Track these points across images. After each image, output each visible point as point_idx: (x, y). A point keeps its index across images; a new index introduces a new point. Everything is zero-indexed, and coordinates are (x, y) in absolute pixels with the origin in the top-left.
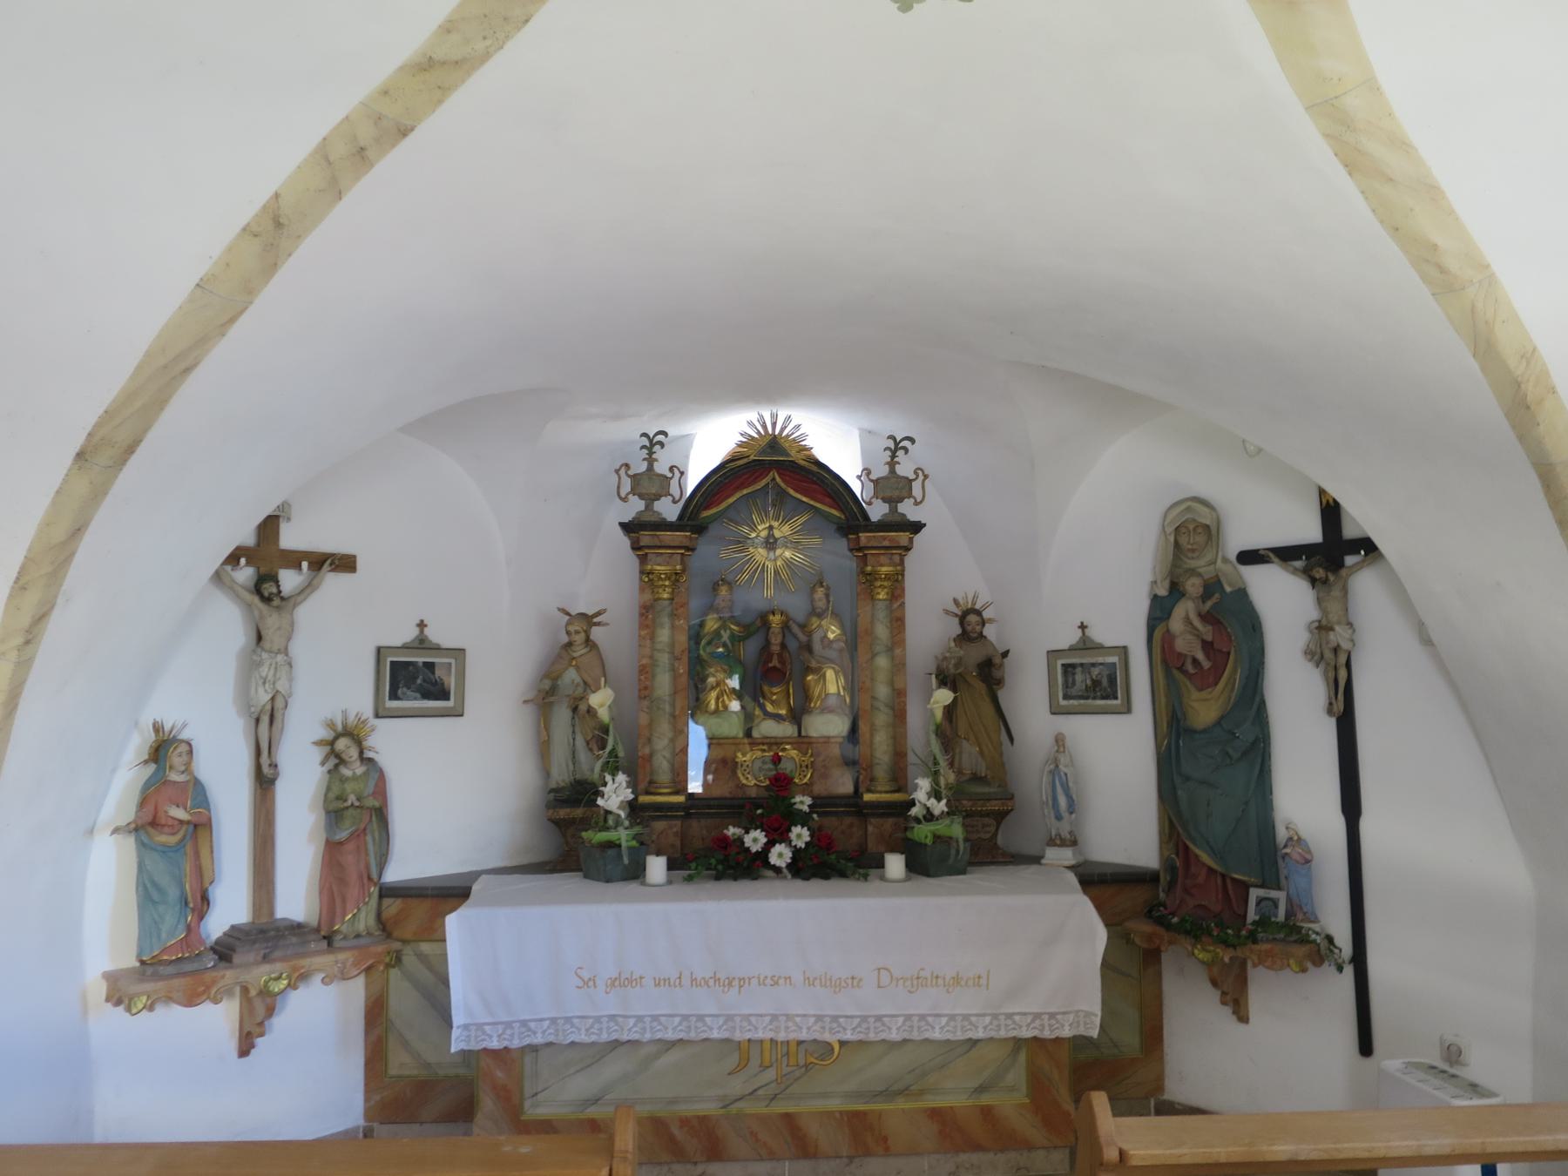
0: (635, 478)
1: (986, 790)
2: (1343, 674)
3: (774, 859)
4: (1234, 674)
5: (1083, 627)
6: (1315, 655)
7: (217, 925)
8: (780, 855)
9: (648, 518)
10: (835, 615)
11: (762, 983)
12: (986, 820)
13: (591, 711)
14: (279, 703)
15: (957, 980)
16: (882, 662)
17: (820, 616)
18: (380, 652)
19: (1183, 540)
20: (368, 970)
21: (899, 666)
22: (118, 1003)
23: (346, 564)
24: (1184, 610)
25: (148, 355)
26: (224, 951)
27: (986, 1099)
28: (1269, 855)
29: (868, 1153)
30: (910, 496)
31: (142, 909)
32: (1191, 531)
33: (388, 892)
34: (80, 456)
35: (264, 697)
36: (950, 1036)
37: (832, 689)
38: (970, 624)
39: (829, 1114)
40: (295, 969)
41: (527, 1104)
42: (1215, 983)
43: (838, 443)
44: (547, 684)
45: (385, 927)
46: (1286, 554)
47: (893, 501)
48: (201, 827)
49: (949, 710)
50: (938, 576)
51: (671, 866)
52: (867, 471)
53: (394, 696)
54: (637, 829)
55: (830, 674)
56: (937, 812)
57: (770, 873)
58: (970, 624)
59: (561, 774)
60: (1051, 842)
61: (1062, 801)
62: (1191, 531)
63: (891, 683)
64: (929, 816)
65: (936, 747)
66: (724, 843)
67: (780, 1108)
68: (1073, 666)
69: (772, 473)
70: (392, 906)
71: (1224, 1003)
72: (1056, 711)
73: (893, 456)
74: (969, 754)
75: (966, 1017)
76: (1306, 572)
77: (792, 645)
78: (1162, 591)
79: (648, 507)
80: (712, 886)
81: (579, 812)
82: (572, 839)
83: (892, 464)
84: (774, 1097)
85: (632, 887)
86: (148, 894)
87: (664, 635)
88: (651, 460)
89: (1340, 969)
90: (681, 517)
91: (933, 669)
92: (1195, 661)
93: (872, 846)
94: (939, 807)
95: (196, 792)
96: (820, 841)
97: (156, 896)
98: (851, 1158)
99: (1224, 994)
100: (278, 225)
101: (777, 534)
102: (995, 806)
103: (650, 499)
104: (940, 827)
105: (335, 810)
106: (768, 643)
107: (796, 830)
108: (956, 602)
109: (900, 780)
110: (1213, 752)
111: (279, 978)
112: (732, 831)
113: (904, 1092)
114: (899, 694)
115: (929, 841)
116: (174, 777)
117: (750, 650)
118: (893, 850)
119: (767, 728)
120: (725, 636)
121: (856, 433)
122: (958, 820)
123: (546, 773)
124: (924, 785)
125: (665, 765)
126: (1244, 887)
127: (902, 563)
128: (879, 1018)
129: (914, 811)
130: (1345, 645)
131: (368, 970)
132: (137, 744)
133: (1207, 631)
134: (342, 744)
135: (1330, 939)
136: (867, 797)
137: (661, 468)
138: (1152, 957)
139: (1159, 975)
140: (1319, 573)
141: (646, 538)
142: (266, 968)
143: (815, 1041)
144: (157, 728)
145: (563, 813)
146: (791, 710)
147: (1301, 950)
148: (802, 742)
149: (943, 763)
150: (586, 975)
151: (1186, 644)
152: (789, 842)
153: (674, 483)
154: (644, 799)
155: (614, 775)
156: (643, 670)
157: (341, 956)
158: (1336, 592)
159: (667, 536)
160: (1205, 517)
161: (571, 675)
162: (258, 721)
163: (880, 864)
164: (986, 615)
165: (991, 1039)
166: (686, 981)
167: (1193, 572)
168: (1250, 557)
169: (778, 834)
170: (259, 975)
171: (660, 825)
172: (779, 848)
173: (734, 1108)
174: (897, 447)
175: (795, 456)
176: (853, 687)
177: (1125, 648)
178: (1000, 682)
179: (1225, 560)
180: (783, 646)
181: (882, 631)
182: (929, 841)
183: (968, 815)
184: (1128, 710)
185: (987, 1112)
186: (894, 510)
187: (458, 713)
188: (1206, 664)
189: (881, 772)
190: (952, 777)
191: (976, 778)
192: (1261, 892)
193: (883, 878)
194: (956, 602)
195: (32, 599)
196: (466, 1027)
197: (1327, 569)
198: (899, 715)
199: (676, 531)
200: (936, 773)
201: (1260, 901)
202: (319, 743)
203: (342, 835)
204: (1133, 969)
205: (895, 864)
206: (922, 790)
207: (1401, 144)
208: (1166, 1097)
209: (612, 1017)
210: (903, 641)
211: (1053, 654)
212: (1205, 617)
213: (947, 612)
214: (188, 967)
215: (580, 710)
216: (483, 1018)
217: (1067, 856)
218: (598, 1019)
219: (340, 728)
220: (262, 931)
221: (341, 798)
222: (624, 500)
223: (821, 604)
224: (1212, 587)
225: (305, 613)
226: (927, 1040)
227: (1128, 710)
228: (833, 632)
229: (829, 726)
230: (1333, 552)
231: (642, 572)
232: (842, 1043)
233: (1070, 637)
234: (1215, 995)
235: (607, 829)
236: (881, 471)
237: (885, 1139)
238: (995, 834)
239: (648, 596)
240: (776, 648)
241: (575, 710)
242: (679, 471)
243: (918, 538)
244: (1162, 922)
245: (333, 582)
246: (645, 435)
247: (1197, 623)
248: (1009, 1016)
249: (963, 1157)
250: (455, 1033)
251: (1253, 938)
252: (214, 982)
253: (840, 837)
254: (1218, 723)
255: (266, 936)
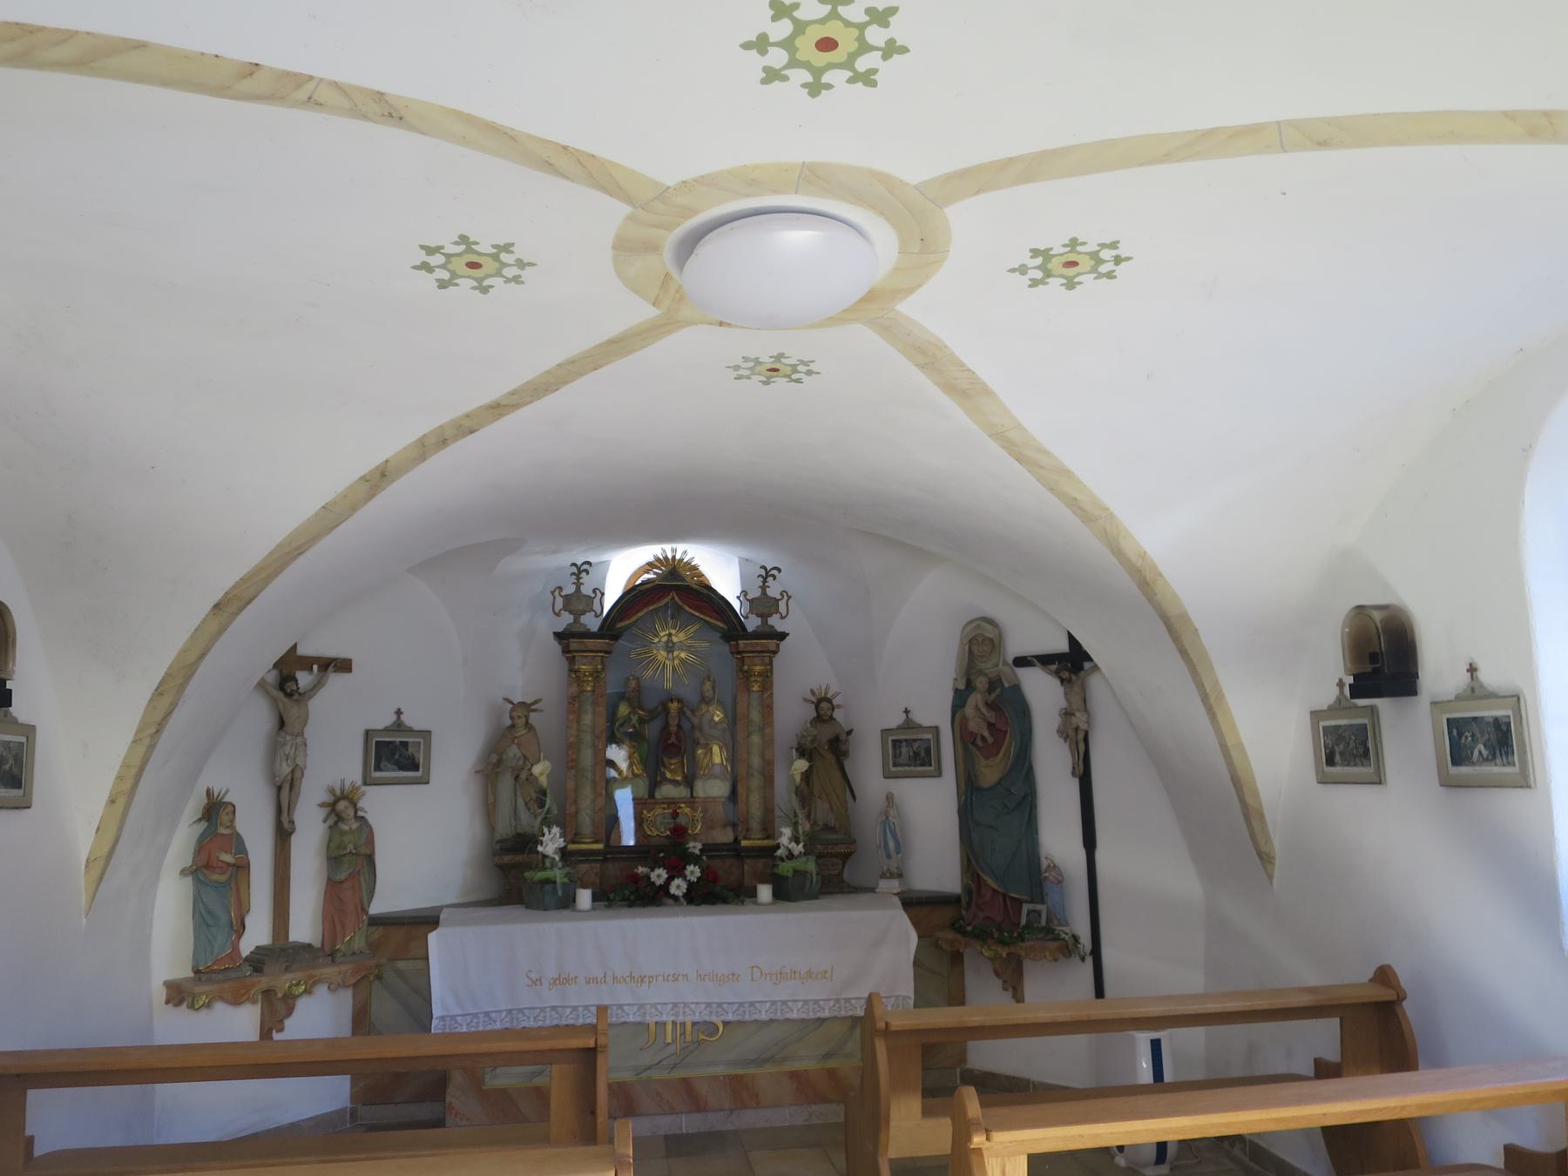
0: (567, 598)
1: (834, 836)
2: (1082, 746)
3: (673, 890)
4: (1010, 746)
5: (906, 711)
6: (1063, 733)
7: (247, 946)
8: (678, 887)
9: (576, 629)
10: (720, 703)
11: (666, 979)
12: (835, 860)
13: (531, 779)
14: (298, 774)
15: (809, 974)
16: (756, 739)
17: (708, 703)
18: (368, 734)
19: (974, 649)
20: (355, 985)
21: (768, 742)
22: (178, 1004)
23: (344, 666)
24: (975, 699)
25: (280, 545)
26: (258, 961)
27: (831, 1064)
28: (1035, 877)
29: (745, 1107)
30: (777, 611)
31: (196, 929)
32: (981, 642)
33: (376, 921)
34: (217, 606)
35: (286, 769)
36: (804, 1016)
37: (717, 760)
38: (823, 707)
39: (715, 1078)
40: (310, 977)
41: (487, 1078)
42: (997, 974)
43: (723, 572)
44: (494, 758)
45: (374, 947)
46: (1045, 660)
47: (764, 617)
48: (242, 868)
49: (807, 776)
50: (801, 670)
51: (595, 898)
52: (744, 593)
53: (378, 768)
54: (568, 869)
55: (716, 749)
56: (796, 853)
57: (670, 901)
58: (823, 707)
59: (504, 829)
60: (883, 876)
61: (891, 844)
62: (981, 642)
63: (762, 755)
64: (791, 856)
65: (796, 804)
66: (636, 879)
67: (679, 1074)
68: (900, 741)
69: (673, 591)
70: (378, 932)
71: (1005, 989)
72: (888, 775)
73: (765, 581)
74: (822, 810)
75: (816, 1002)
76: (1057, 673)
77: (686, 726)
78: (962, 687)
79: (576, 620)
80: (625, 911)
81: (519, 858)
82: (514, 877)
83: (764, 588)
84: (675, 1066)
85: (565, 913)
86: (203, 918)
87: (587, 719)
88: (578, 585)
89: (1083, 959)
90: (601, 628)
91: (795, 745)
92: (983, 738)
93: (747, 881)
94: (798, 849)
95: (237, 843)
96: (708, 876)
97: (210, 921)
98: (732, 1111)
99: (1005, 982)
100: (383, 475)
101: (675, 639)
102: (841, 849)
103: (578, 614)
104: (798, 864)
105: (335, 857)
106: (667, 725)
107: (690, 868)
108: (812, 692)
109: (769, 831)
110: (997, 804)
111: (298, 984)
112: (641, 870)
113: (770, 1060)
114: (768, 764)
115: (790, 875)
116: (222, 830)
117: (652, 730)
118: (763, 882)
119: (667, 791)
120: (634, 719)
121: (736, 561)
122: (812, 858)
123: (491, 828)
124: (787, 832)
125: (588, 821)
126: (1020, 902)
127: (771, 663)
128: (752, 1004)
129: (779, 852)
130: (1083, 726)
131: (355, 985)
132: (194, 806)
133: (990, 716)
134: (342, 805)
135: (1076, 939)
136: (744, 843)
137: (586, 590)
138: (957, 959)
139: (962, 973)
140: (1066, 675)
141: (574, 644)
142: (289, 976)
143: (705, 1022)
144: (209, 793)
145: (507, 859)
146: (685, 777)
147: (1054, 945)
148: (692, 801)
149: (801, 816)
150: (534, 976)
151: (976, 725)
152: (684, 877)
153: (596, 601)
154: (572, 847)
155: (549, 828)
156: (570, 746)
157: (344, 968)
158: (1076, 689)
159: (590, 642)
160: (989, 632)
161: (513, 751)
162: (279, 788)
163: (753, 894)
164: (835, 702)
165: (835, 1018)
166: (609, 979)
167: (981, 672)
168: (1022, 662)
169: (676, 871)
170: (284, 982)
171: (584, 867)
172: (677, 881)
173: (644, 1075)
174: (767, 575)
175: (693, 582)
176: (733, 758)
177: (937, 728)
178: (846, 754)
179: (1005, 663)
180: (679, 726)
181: (755, 715)
182: (790, 875)
183: (819, 856)
184: (939, 774)
185: (831, 1073)
186: (765, 622)
187: (425, 781)
188: (990, 740)
189: (755, 824)
190: (808, 827)
191: (827, 828)
192: (1031, 906)
193: (756, 903)
194: (812, 692)
195: (166, 701)
196: (442, 1018)
197: (1070, 671)
198: (769, 780)
199: (594, 641)
200: (796, 824)
201: (1029, 912)
202: (322, 805)
203: (342, 876)
204: (940, 971)
205: (765, 892)
206: (785, 836)
207: (1046, 453)
208: (968, 1066)
209: (554, 1008)
210: (771, 724)
211: (885, 732)
212: (990, 706)
213: (805, 700)
214: (233, 975)
215: (521, 776)
216: (457, 1011)
217: (894, 885)
218: (543, 1010)
219: (338, 792)
220: (283, 950)
221: (341, 846)
222: (558, 615)
223: (709, 694)
224: (994, 684)
225: (316, 705)
226: (788, 1020)
227: (939, 774)
228: (718, 716)
229: (714, 789)
230: (1072, 663)
231: (570, 670)
232: (725, 1023)
233: (896, 720)
234: (998, 983)
235: (545, 869)
236: (755, 593)
237: (757, 1096)
238: (841, 872)
239: (574, 689)
240: (673, 729)
241: (517, 778)
242: (599, 592)
243: (783, 644)
244: (961, 931)
245: (335, 680)
246: (574, 564)
247: (984, 710)
248: (848, 1000)
249: (814, 1108)
250: (434, 1023)
251: (1021, 938)
252: (253, 986)
253: (723, 876)
254: (999, 783)
255: (282, 953)
